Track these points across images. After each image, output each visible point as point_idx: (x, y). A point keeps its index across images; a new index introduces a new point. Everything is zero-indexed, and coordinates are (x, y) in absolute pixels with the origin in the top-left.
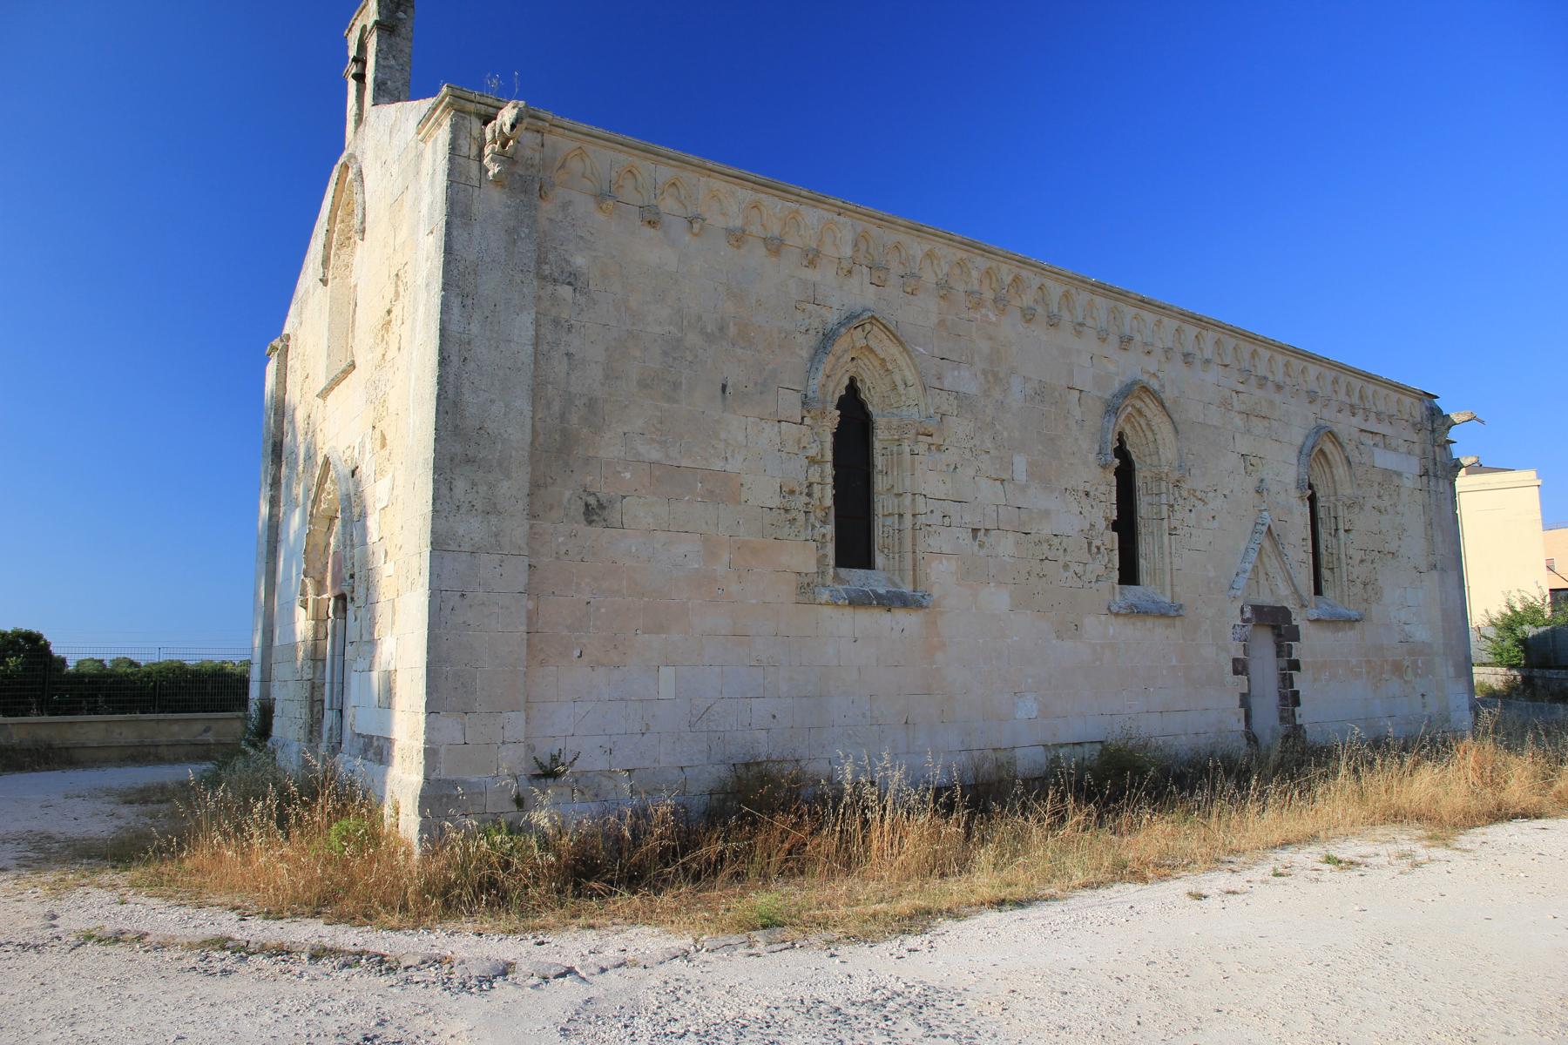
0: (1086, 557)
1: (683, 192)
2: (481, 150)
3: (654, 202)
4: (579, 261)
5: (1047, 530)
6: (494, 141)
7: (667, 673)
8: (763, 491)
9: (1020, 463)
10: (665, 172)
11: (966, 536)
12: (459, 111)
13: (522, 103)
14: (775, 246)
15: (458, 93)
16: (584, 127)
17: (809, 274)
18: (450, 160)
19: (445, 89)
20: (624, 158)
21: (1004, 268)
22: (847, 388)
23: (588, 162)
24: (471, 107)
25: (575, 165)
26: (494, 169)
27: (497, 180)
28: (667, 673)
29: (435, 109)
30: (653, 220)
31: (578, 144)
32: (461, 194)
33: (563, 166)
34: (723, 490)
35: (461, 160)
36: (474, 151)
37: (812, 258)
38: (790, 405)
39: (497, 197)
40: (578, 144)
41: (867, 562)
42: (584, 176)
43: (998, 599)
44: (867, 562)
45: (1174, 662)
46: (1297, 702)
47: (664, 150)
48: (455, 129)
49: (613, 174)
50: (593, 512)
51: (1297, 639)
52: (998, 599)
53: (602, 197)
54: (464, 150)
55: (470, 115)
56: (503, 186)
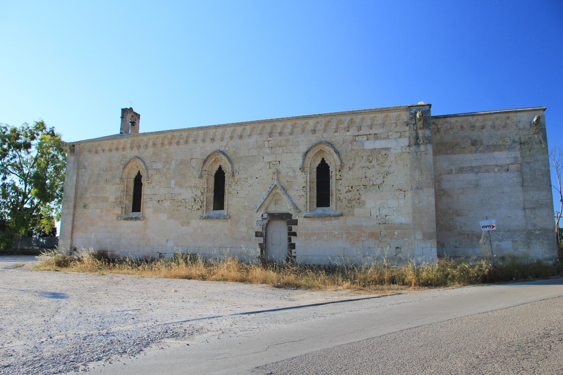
0: (193, 203)
4: (86, 164)
5: (180, 198)
7: (93, 234)
8: (112, 199)
9: (173, 182)
11: (156, 203)
14: (117, 149)
17: (124, 153)
21: (168, 135)
22: (321, 162)
28: (93, 234)
30: (97, 152)
34: (105, 200)
37: (124, 149)
38: (118, 180)
41: (222, 208)
43: (164, 217)
44: (222, 208)
45: (227, 232)
46: (294, 248)
50: (85, 207)
51: (297, 225)
52: (164, 217)
53: (90, 151)
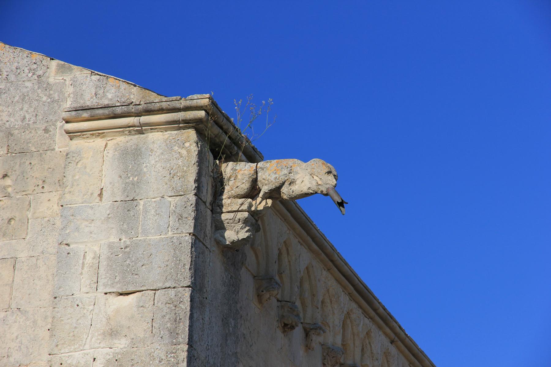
6: (253, 192)
19: (203, 100)
29: (149, 112)
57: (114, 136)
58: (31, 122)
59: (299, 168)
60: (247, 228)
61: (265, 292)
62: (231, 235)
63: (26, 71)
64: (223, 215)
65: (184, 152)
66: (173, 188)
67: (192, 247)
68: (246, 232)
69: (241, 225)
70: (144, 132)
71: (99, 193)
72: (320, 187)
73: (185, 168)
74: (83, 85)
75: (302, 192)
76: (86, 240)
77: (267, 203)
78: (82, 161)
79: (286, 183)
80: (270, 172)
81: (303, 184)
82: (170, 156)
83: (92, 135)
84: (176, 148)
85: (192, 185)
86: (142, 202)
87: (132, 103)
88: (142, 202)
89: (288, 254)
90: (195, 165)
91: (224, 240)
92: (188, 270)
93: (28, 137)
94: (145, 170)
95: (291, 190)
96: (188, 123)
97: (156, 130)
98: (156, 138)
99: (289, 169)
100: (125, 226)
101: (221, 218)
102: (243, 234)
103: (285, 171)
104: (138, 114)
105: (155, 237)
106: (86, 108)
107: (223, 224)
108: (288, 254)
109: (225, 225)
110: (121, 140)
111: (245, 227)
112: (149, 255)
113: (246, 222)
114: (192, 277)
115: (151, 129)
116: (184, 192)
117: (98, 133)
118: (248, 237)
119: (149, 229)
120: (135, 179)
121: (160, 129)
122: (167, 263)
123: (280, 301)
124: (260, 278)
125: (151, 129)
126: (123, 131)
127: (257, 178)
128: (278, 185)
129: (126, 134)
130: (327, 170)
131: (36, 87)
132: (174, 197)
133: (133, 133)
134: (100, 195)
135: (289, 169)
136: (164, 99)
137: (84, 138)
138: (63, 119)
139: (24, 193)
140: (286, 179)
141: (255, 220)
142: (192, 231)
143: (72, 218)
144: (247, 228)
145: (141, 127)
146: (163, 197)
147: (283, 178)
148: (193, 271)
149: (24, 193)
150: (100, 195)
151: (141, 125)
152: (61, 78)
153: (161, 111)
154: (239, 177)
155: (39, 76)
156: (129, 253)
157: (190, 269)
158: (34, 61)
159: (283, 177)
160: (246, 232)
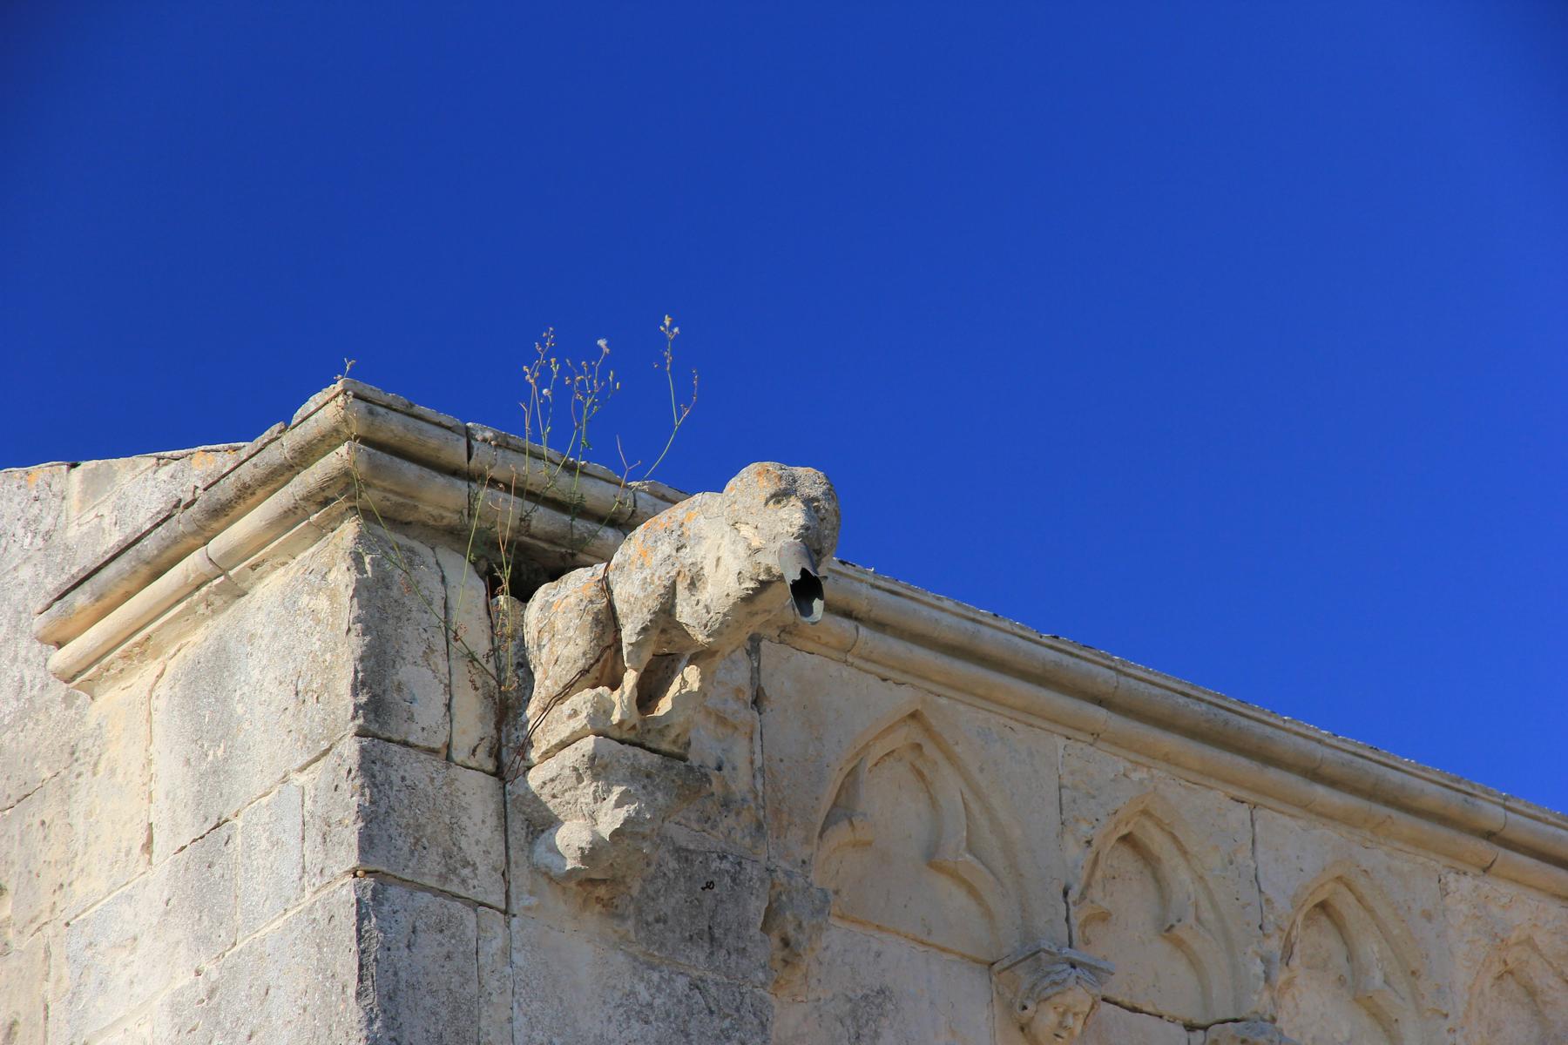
1: (1371, 948)
2: (507, 709)
3: (1260, 1001)
6: (602, 667)
10: (1297, 849)
12: (387, 515)
13: (810, 480)
15: (394, 427)
16: (944, 614)
18: (370, 768)
19: (326, 408)
20: (1119, 775)
23: (950, 787)
24: (442, 498)
25: (891, 806)
26: (586, 820)
27: (601, 880)
29: (222, 513)
31: (903, 698)
32: (429, 945)
33: (843, 809)
35: (418, 770)
36: (471, 725)
39: (584, 960)
40: (903, 698)
42: (932, 859)
47: (1294, 735)
48: (378, 607)
49: (1074, 852)
54: (425, 718)
55: (471, 548)
56: (610, 908)
57: (179, 636)
58: (35, 692)
59: (702, 520)
60: (617, 790)
61: (1031, 1007)
62: (571, 837)
63: (20, 532)
64: (532, 773)
65: (322, 603)
66: (305, 737)
67: (361, 917)
68: (619, 804)
69: (588, 788)
70: (245, 585)
71: (144, 839)
72: (760, 557)
73: (328, 656)
74: (136, 489)
75: (731, 600)
76: (119, 1015)
77: (684, 682)
78: (104, 757)
79: (680, 588)
80: (635, 571)
81: (722, 569)
82: (297, 614)
83: (126, 657)
84: (305, 599)
85: (344, 700)
86: (239, 822)
87: (176, 506)
88: (239, 822)
89: (1184, 853)
90: (353, 634)
91: (557, 860)
92: (352, 1000)
93: (31, 741)
94: (240, 709)
95: (701, 605)
96: (320, 498)
97: (266, 566)
98: (270, 588)
99: (675, 535)
100: (206, 922)
101: (527, 788)
102: (610, 819)
103: (666, 548)
104: (203, 533)
105: (273, 926)
106: (82, 575)
107: (542, 804)
108: (1184, 853)
109: (550, 805)
110: (199, 639)
111: (609, 791)
112: (263, 992)
113: (597, 767)
114: (371, 1022)
115: (253, 567)
116: (328, 738)
117: (136, 645)
118: (627, 821)
119: (257, 904)
120: (220, 753)
121: (273, 555)
122: (305, 1001)
123: (1205, 1028)
124: (1006, 963)
125: (253, 567)
126: (190, 610)
127: (611, 606)
128: (654, 604)
129: (205, 617)
130: (769, 488)
131: (42, 572)
132: (312, 768)
133: (218, 602)
134: (148, 846)
135: (675, 535)
136: (248, 447)
137: (115, 678)
138: (42, 640)
139: (35, 926)
140: (673, 573)
141: (643, 752)
142: (353, 861)
143: (89, 953)
144: (617, 790)
145: (224, 572)
146: (285, 780)
147: (662, 576)
148: (371, 998)
149: (35, 926)
150: (148, 846)
151: (220, 567)
152: (92, 514)
153: (246, 495)
154: (559, 625)
155: (47, 536)
156: (217, 1008)
157: (359, 994)
158: (34, 493)
159: (662, 571)
160: (619, 804)
